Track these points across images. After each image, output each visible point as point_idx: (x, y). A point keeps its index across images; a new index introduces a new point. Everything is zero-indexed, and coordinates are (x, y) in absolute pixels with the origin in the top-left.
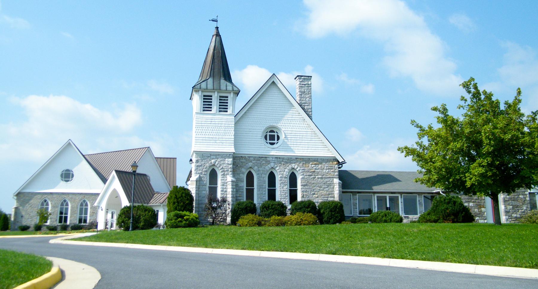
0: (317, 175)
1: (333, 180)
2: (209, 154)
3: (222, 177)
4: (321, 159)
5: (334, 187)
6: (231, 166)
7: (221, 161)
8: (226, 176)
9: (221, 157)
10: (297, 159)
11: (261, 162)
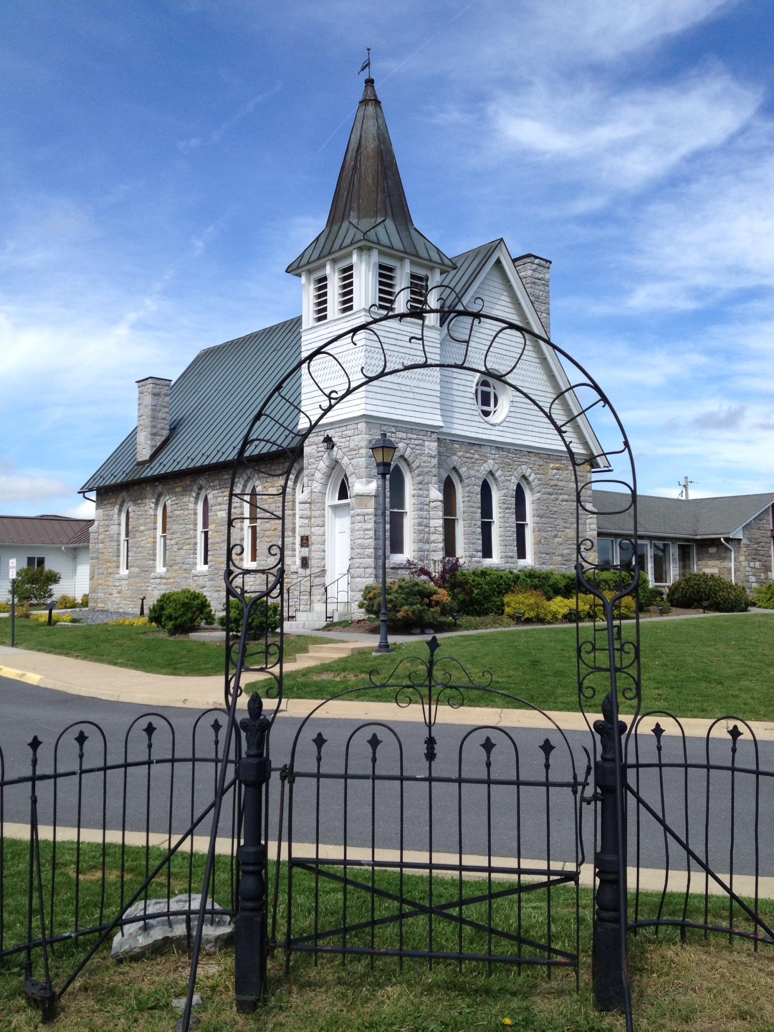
0: (560, 494)
6: (435, 461)
9: (415, 436)
10: (530, 454)
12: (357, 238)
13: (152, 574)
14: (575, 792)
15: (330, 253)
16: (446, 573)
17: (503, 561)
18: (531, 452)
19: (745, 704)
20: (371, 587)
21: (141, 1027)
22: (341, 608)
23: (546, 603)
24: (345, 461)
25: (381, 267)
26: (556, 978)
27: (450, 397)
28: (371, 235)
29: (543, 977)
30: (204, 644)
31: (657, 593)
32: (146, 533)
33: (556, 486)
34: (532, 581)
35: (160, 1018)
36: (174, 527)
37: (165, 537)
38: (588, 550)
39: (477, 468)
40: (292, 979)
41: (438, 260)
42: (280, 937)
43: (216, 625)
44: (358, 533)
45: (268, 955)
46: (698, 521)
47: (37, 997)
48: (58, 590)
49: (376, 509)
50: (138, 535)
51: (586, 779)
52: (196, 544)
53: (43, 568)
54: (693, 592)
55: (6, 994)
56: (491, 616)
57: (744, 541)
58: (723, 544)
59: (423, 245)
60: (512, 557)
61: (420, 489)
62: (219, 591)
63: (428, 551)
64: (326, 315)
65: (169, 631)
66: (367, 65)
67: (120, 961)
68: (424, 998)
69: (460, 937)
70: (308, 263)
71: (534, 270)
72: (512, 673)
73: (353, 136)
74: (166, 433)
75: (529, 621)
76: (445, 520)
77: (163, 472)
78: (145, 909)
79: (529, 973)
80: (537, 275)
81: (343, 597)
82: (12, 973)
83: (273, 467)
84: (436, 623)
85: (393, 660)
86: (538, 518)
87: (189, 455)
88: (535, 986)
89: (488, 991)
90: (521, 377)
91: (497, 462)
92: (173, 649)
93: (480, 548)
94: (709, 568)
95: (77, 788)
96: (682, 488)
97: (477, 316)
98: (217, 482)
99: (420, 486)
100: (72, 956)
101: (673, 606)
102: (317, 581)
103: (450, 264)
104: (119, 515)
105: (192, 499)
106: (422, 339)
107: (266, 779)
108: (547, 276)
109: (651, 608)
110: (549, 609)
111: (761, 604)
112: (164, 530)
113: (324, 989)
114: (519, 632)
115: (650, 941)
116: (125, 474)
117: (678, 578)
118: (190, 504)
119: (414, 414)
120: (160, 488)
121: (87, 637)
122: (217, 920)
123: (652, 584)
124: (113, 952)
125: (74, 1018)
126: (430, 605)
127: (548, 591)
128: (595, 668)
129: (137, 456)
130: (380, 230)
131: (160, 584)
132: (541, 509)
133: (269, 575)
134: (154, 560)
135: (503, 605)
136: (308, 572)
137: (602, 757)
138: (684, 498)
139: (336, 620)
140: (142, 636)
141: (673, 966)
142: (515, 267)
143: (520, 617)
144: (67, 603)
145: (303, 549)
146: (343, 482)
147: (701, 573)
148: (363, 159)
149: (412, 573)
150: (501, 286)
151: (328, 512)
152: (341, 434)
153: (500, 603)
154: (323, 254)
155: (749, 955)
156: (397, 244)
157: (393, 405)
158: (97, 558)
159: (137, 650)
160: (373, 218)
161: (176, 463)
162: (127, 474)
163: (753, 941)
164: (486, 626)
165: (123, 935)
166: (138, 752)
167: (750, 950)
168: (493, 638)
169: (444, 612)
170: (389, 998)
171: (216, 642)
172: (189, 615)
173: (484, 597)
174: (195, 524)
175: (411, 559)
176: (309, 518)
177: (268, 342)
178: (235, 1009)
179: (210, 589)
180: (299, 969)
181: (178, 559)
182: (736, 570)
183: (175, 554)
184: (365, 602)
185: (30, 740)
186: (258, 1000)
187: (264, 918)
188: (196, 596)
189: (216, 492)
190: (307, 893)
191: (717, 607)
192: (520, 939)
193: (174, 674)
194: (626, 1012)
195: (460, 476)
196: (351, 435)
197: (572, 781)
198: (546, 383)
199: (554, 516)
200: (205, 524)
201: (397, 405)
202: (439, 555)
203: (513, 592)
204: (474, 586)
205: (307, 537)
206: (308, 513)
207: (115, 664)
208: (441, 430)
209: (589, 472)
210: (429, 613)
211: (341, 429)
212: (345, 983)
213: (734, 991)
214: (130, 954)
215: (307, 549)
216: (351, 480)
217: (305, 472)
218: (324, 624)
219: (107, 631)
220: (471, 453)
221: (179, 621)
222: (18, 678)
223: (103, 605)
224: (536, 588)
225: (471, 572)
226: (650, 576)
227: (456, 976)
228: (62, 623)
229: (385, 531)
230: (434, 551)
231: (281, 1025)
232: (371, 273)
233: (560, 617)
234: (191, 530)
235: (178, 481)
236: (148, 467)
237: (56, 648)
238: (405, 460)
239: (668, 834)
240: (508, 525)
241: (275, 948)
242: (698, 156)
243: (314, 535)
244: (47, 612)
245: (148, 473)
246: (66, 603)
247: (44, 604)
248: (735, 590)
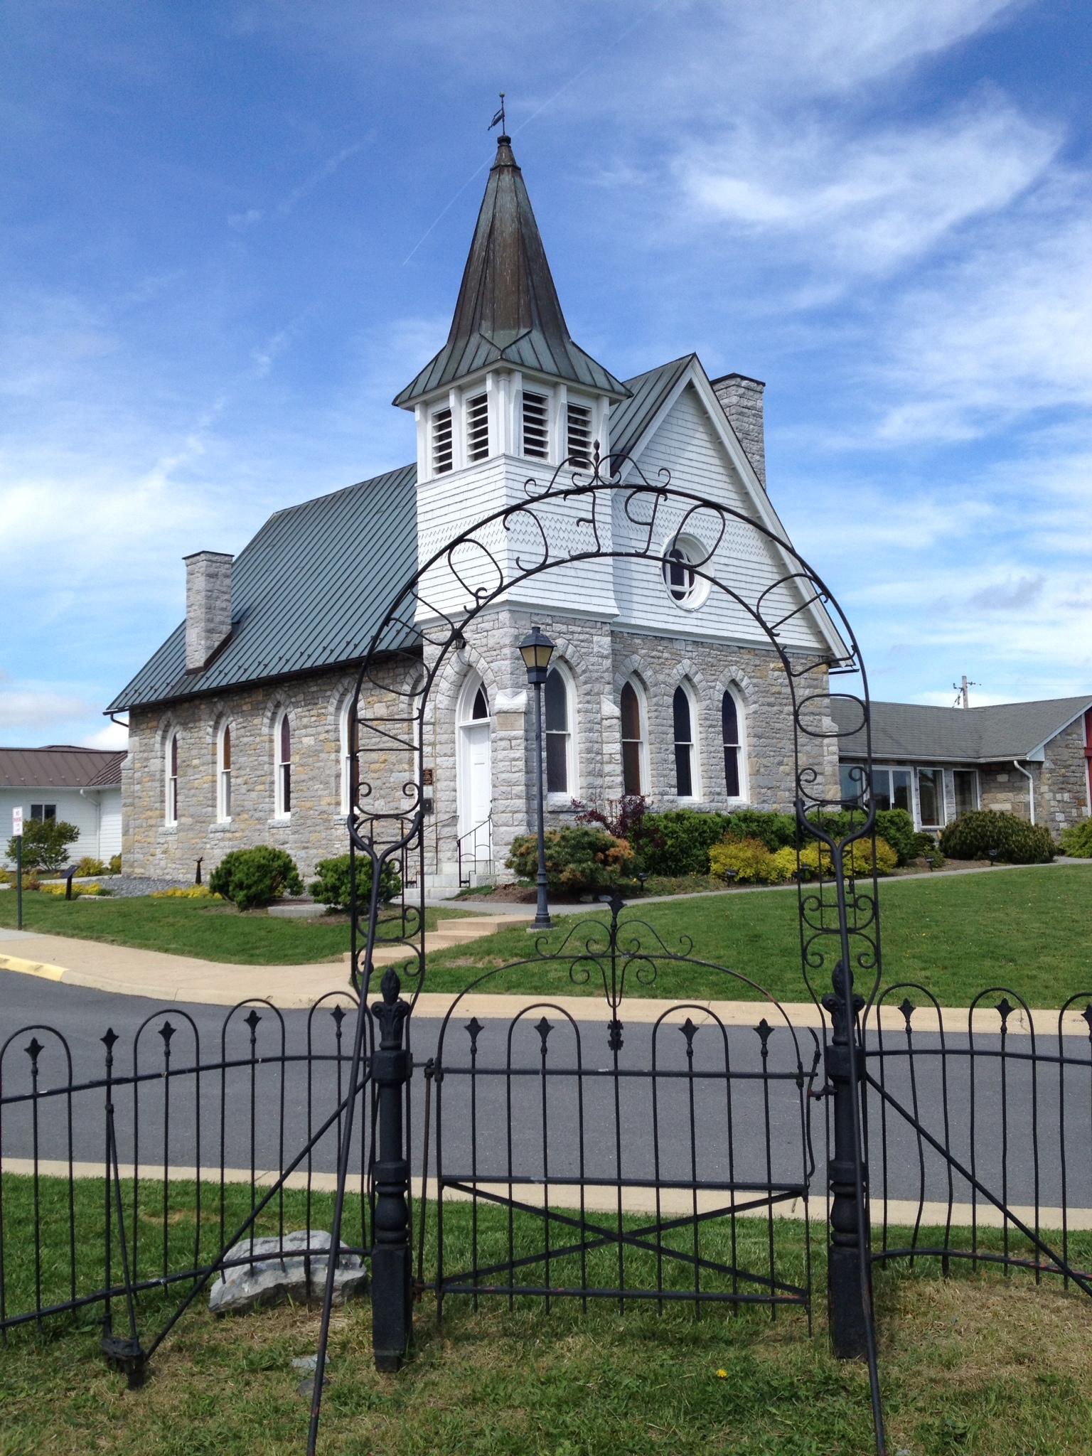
6: (607, 663)
9: (579, 629)
10: (742, 651)
12: (492, 358)
13: (212, 826)
14: (800, 1085)
15: (454, 379)
16: (627, 817)
17: (707, 799)
18: (743, 648)
19: (1046, 987)
20: (522, 839)
21: (255, 1391)
22: (481, 868)
23: (768, 856)
24: (482, 665)
25: (527, 396)
26: (783, 1323)
27: (627, 574)
28: (512, 353)
29: (766, 1322)
30: (290, 921)
31: (926, 839)
32: (201, 768)
33: (779, 693)
34: (748, 827)
35: (279, 1382)
36: (242, 760)
37: (228, 773)
38: (810, 782)
39: (667, 671)
40: (444, 1331)
42: (430, 1275)
43: (305, 895)
44: (501, 764)
45: (413, 1299)
46: (981, 738)
47: (120, 1356)
48: (76, 851)
49: (526, 731)
51: (814, 1068)
52: (273, 783)
53: (54, 820)
54: (975, 837)
55: (78, 1356)
56: (691, 877)
57: (1047, 765)
58: (1017, 770)
59: (584, 365)
60: (719, 794)
61: (588, 702)
62: (307, 848)
63: (601, 787)
64: (451, 463)
65: (240, 904)
66: (500, 118)
67: (220, 1316)
68: (615, 1349)
69: (659, 1278)
70: (424, 392)
71: (741, 396)
72: (722, 953)
73: (483, 217)
74: (226, 629)
75: (744, 882)
76: (625, 745)
77: (224, 683)
78: (251, 1250)
79: (749, 1318)
80: (745, 403)
81: (483, 854)
82: (82, 1333)
83: (380, 675)
84: (614, 887)
85: (557, 938)
86: (755, 739)
87: (260, 659)
88: (756, 1333)
89: (696, 1340)
91: (696, 662)
92: (247, 930)
93: (674, 782)
94: (999, 803)
95: (133, 1114)
96: (958, 693)
97: (662, 491)
98: (301, 697)
99: (588, 698)
100: (158, 1311)
101: (947, 856)
102: (446, 832)
103: (623, 390)
104: (163, 743)
105: (266, 721)
106: (593, 521)
107: (406, 1077)
108: (759, 404)
109: (917, 860)
110: (772, 865)
111: (1072, 851)
112: (227, 764)
113: (486, 1342)
114: (731, 898)
115: (903, 1277)
116: (169, 687)
117: (954, 817)
118: (263, 728)
119: (577, 598)
120: (220, 706)
121: (124, 915)
122: (344, 1262)
123: (917, 827)
124: (211, 1305)
125: (172, 1383)
126: (605, 862)
127: (771, 840)
128: (822, 929)
130: (524, 344)
131: (222, 840)
132: (759, 727)
133: (406, 821)
134: (214, 806)
135: (708, 860)
137: (834, 1041)
138: (961, 706)
139: (474, 885)
140: (201, 912)
141: (933, 1304)
142: (714, 392)
143: (733, 877)
144: (90, 868)
146: (479, 694)
147: (987, 810)
148: (497, 247)
149: (580, 818)
150: (696, 420)
151: (460, 736)
152: (474, 627)
153: (703, 858)
154: (443, 381)
155: (1030, 1290)
156: (548, 364)
158: (132, 805)
159: (196, 931)
160: (514, 328)
161: (242, 671)
162: (173, 687)
163: (1034, 1271)
164: (684, 890)
165: (224, 1282)
166: (239, 1051)
167: (1032, 1284)
168: (695, 906)
169: (625, 872)
170: (569, 1350)
171: (307, 918)
172: (268, 882)
173: (681, 851)
174: (272, 756)
175: (578, 800)
177: (366, 503)
178: (373, 1368)
179: (294, 845)
180: (452, 1320)
181: (248, 805)
182: (1037, 805)
183: (244, 797)
184: (515, 859)
185: (104, 1034)
186: (403, 1355)
187: (408, 1252)
188: (276, 856)
189: (300, 710)
190: (456, 1233)
191: (1010, 857)
192: (738, 1274)
193: (251, 963)
194: (871, 1356)
196: (488, 628)
197: (796, 1071)
198: (761, 552)
199: (778, 735)
200: (286, 755)
201: (553, 587)
202: (617, 793)
203: (722, 842)
204: (667, 835)
205: (430, 771)
207: (166, 951)
208: (615, 619)
209: (825, 673)
210: (605, 873)
212: (512, 1334)
213: (1009, 1332)
214: (234, 1306)
216: (489, 691)
218: (457, 891)
219: (152, 905)
220: (659, 651)
221: (253, 890)
222: (32, 973)
223: (142, 870)
224: (753, 835)
225: (662, 815)
226: (916, 817)
227: (655, 1324)
228: (87, 896)
229: (541, 761)
230: (609, 788)
231: (434, 1384)
232: (512, 406)
233: (788, 875)
234: (265, 763)
236: (202, 677)
237: (82, 930)
238: (566, 662)
239: (922, 1138)
240: (713, 749)
241: (423, 1290)
242: (973, 223)
243: (441, 768)
244: (65, 881)
245: (202, 685)
246: (89, 869)
247: (57, 871)
248: (1034, 832)
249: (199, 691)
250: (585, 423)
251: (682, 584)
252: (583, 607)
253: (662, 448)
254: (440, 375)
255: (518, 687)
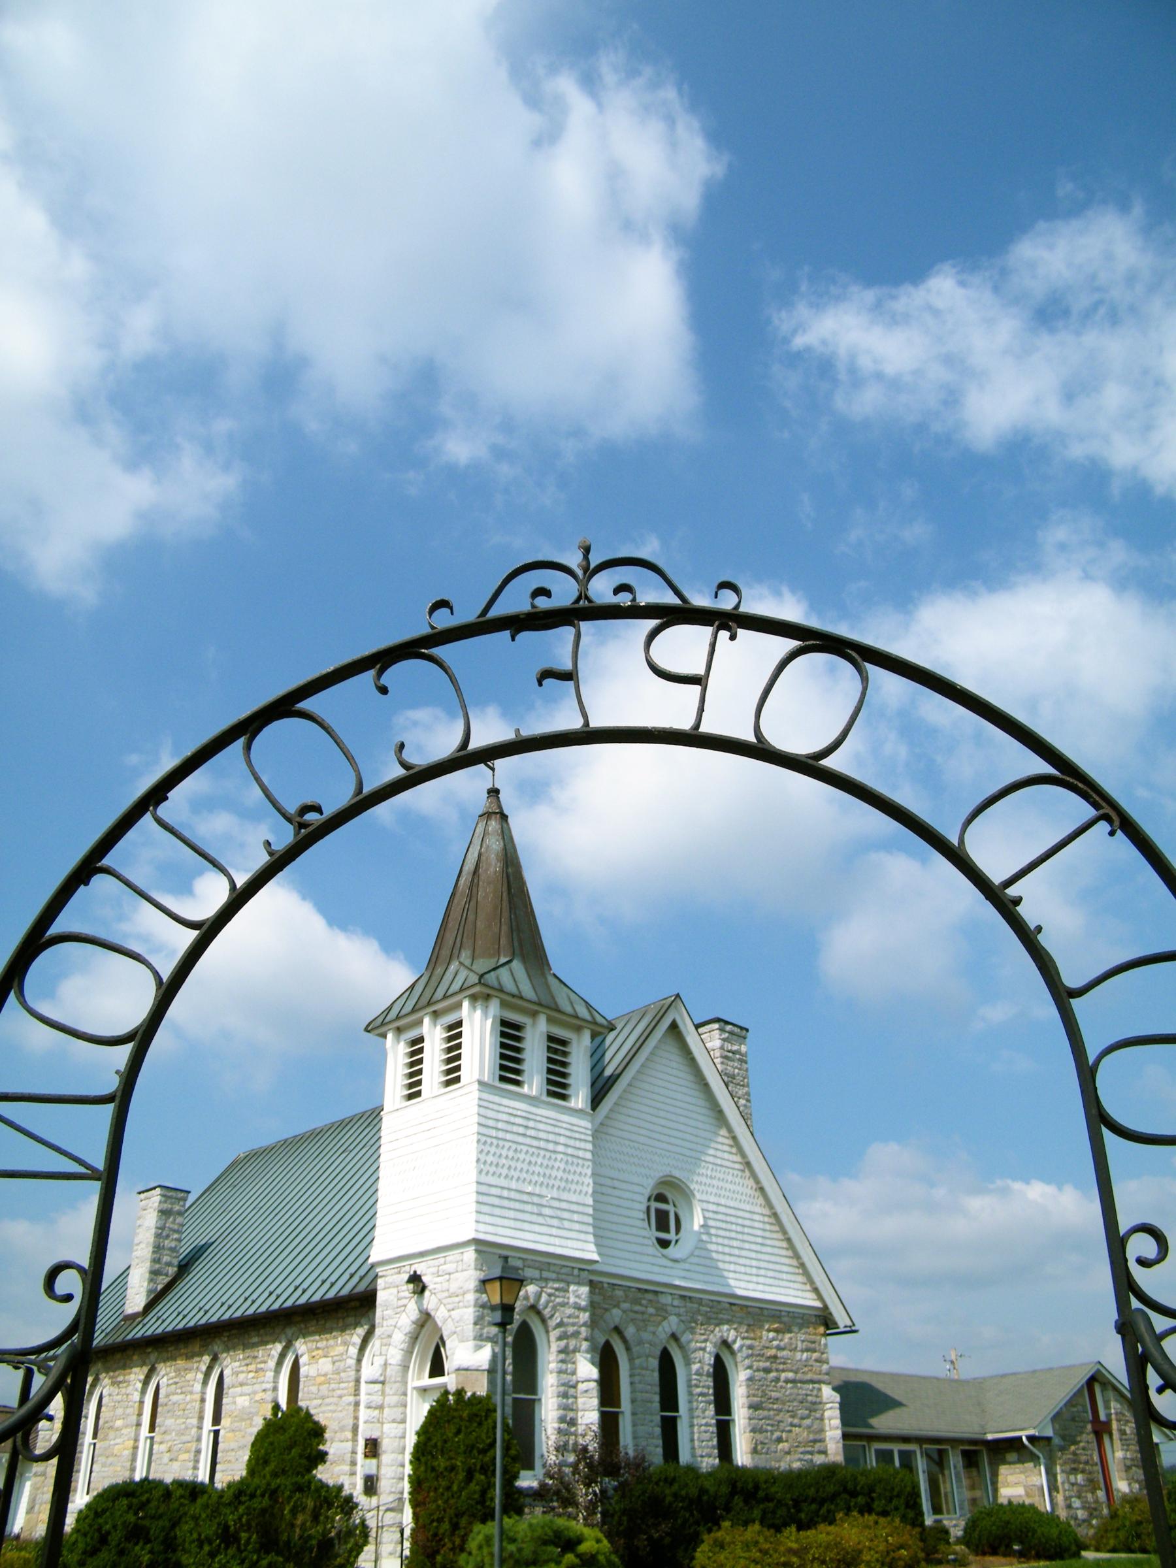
0: (783, 1371)
1: (820, 1390)
2: (519, 1258)
3: (562, 1361)
4: (789, 1312)
5: (823, 1415)
6: (585, 1317)
7: (557, 1293)
8: (571, 1355)
9: (554, 1276)
10: (734, 1308)
11: (643, 1309)
15: (429, 1004)
24: (440, 1315)
25: (504, 1023)
41: (587, 1016)
50: (112, 1434)
74: (172, 1271)
87: (201, 1304)
90: (715, 1190)
108: (743, 1049)
129: (126, 1306)
130: (504, 973)
132: (754, 1395)
136: (374, 1501)
142: (700, 1035)
145: (368, 1461)
156: (527, 990)
157: (519, 1225)
162: (107, 1334)
176: (381, 1407)
189: (237, 1364)
195: (624, 1340)
196: (452, 1270)
200: (217, 1419)
201: (526, 1226)
206: (377, 1399)
211: (436, 1262)
215: (374, 1461)
217: (378, 1331)
235: (181, 1345)
245: (138, 1332)
249: (133, 1339)
250: (565, 1054)
251: (667, 1230)
252: (559, 1251)
253: (646, 1086)
254: (415, 1001)
255: (482, 1340)
